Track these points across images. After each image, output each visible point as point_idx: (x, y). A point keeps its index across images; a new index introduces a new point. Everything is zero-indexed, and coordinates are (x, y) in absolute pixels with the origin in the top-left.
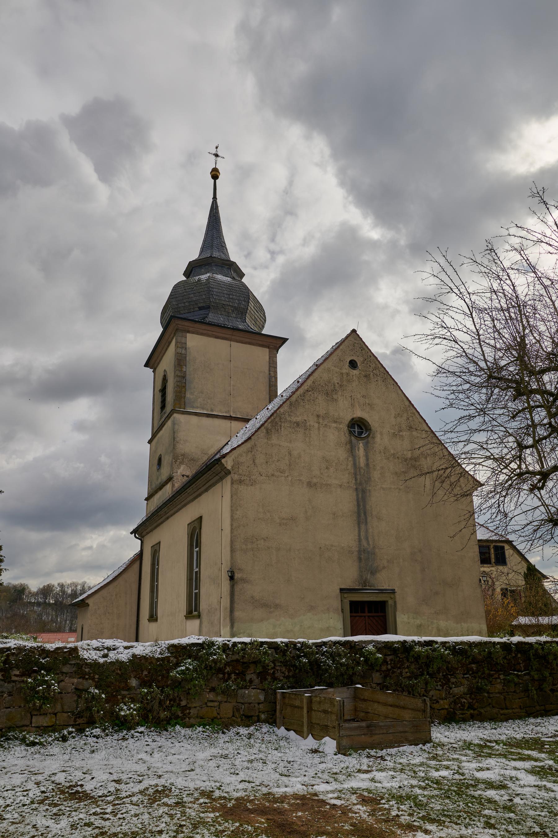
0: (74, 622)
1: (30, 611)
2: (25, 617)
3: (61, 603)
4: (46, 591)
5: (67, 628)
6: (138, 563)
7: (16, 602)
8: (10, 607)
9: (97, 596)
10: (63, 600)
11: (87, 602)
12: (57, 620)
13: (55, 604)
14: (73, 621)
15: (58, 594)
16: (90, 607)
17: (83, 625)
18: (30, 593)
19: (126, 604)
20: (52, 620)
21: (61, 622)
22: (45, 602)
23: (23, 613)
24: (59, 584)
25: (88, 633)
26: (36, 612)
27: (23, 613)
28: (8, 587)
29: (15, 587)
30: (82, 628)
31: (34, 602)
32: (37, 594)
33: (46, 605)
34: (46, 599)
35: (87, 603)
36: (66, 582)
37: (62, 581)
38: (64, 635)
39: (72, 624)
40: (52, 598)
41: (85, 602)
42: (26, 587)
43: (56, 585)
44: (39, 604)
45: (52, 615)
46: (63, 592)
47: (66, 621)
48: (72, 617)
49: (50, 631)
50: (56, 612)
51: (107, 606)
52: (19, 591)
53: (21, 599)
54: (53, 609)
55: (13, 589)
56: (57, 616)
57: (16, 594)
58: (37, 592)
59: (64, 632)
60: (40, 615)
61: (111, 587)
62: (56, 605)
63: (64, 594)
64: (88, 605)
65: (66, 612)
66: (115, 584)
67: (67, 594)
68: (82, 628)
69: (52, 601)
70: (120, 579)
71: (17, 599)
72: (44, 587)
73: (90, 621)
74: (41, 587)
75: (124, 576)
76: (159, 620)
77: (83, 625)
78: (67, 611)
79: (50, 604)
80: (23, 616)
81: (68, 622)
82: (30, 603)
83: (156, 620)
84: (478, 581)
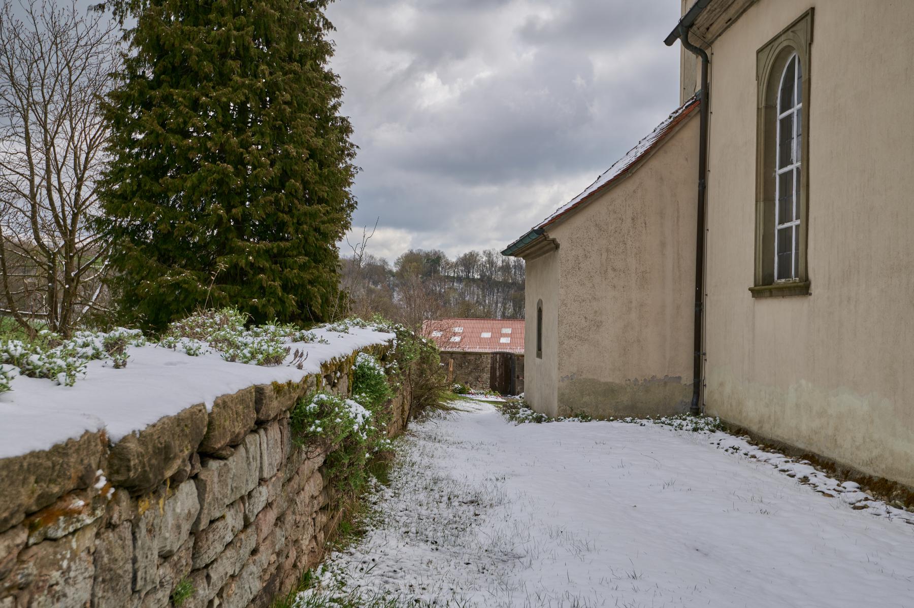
0: (507, 306)
2: (443, 296)
3: (489, 278)
4: (468, 261)
5: (499, 314)
6: (695, 125)
7: (430, 276)
8: (423, 282)
9: (579, 220)
10: (492, 274)
11: (552, 236)
12: (485, 301)
13: (481, 279)
14: (506, 304)
16: (561, 251)
17: (540, 303)
18: (447, 263)
19: (663, 245)
20: (477, 302)
22: (468, 277)
23: (440, 291)
24: (484, 252)
25: (560, 323)
27: (440, 291)
28: (418, 254)
29: (427, 255)
30: (540, 311)
31: (454, 277)
32: (456, 265)
33: (470, 281)
34: (469, 272)
35: (554, 241)
36: (494, 249)
37: (488, 248)
38: (496, 324)
39: (505, 308)
42: (441, 255)
43: (481, 253)
44: (459, 279)
45: (478, 295)
46: (491, 262)
47: (497, 303)
48: (504, 299)
49: (476, 317)
50: (483, 291)
51: (608, 250)
53: (436, 272)
54: (478, 287)
55: (425, 257)
56: (484, 296)
60: (462, 295)
61: (618, 194)
62: (482, 281)
64: (557, 247)
65: (496, 291)
66: (629, 186)
68: (540, 311)
69: (477, 276)
70: (644, 175)
71: (431, 272)
72: (465, 255)
73: (562, 291)
77: (540, 303)
78: (498, 290)
79: (474, 280)
81: (499, 305)
82: (448, 277)
84: (138, 349)
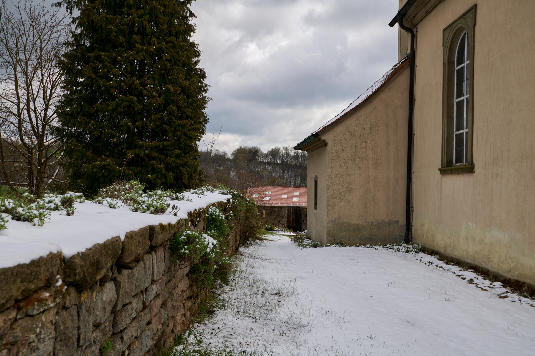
0: (297, 179)
1: (262, 169)
3: (286, 163)
4: (274, 153)
5: (292, 184)
7: (252, 161)
8: (248, 165)
9: (339, 129)
11: (323, 138)
12: (284, 176)
14: (296, 178)
15: (284, 156)
16: (329, 147)
17: (316, 177)
18: (262, 154)
19: (388, 143)
20: (279, 177)
21: (287, 178)
22: (274, 162)
23: (258, 170)
25: (328, 189)
26: (267, 170)
27: (258, 170)
31: (266, 162)
32: (267, 155)
34: (275, 159)
35: (324, 141)
36: (289, 146)
37: (285, 145)
38: (290, 190)
39: (295, 181)
40: (279, 159)
41: (319, 139)
42: (258, 149)
43: (282, 148)
44: (269, 164)
46: (287, 154)
47: (291, 178)
48: (295, 175)
51: (356, 147)
52: (254, 153)
53: (255, 159)
54: (280, 168)
56: (283, 174)
57: (251, 155)
58: (267, 154)
59: (290, 186)
60: (270, 173)
61: (362, 113)
62: (282, 165)
63: (288, 156)
67: (290, 156)
69: (279, 162)
70: (377, 102)
71: (252, 159)
72: (272, 150)
73: (329, 171)
74: (270, 150)
75: (383, 96)
76: (476, 169)
77: (316, 177)
78: (292, 170)
79: (277, 164)
80: (258, 173)
81: (292, 179)
82: (262, 162)
83: (470, 169)
